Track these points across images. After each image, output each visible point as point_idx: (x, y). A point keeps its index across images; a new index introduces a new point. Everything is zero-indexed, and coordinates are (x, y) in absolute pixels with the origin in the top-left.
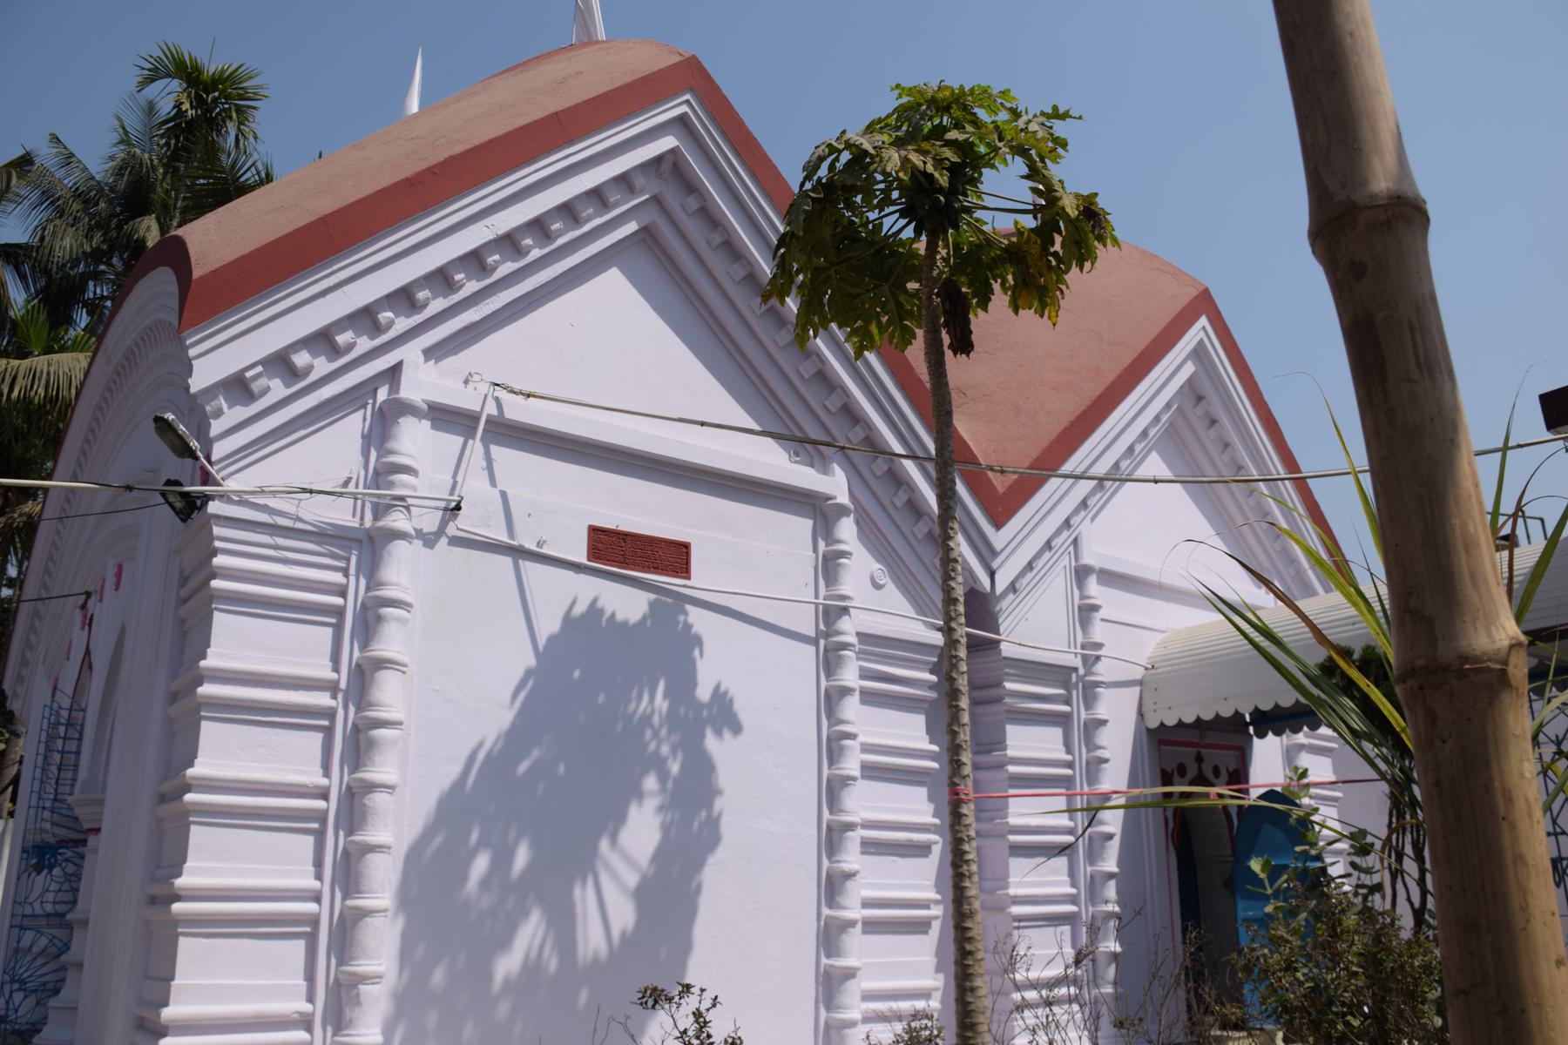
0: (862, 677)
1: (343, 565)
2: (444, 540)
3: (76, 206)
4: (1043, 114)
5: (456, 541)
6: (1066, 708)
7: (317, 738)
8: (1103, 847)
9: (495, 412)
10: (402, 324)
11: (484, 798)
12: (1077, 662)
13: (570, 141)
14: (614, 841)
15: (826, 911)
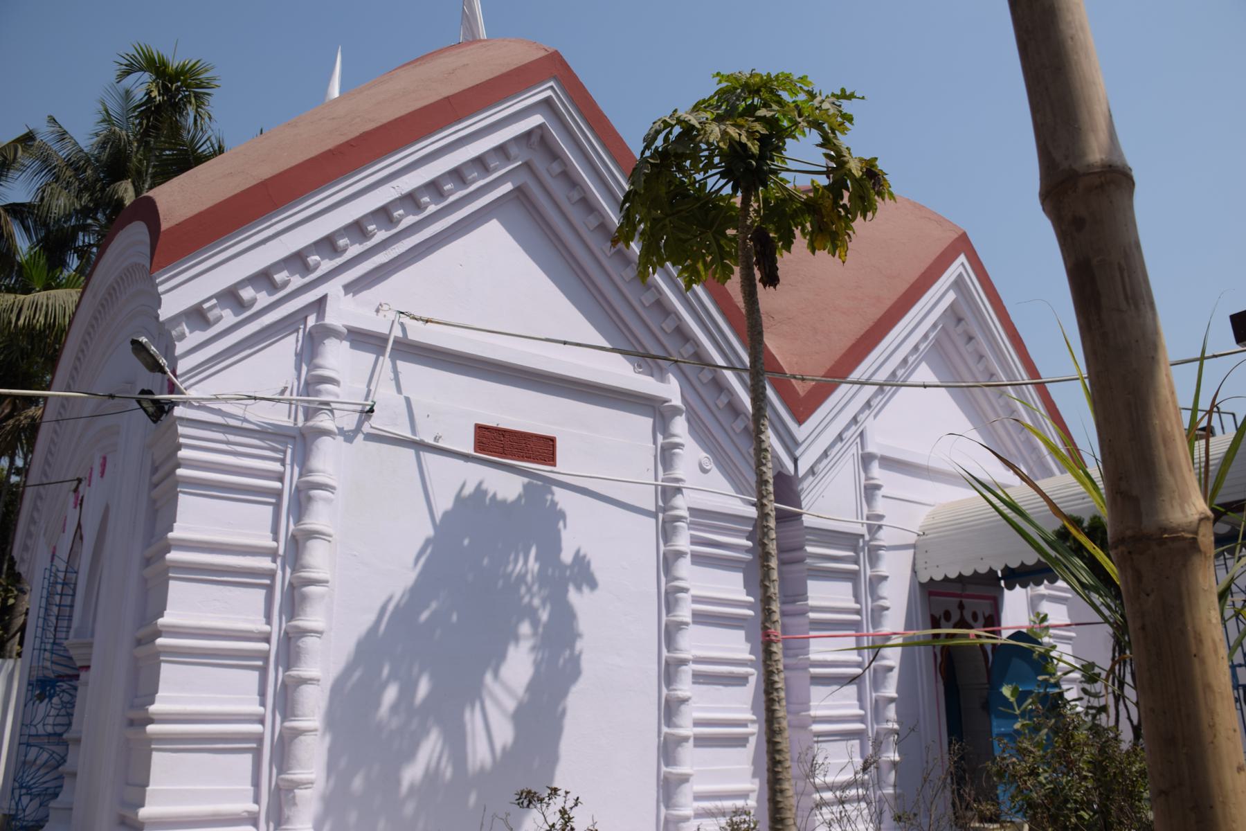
0: (693, 543)
1: (280, 456)
2: (360, 437)
3: (68, 173)
4: (833, 95)
5: (370, 437)
7: (262, 593)
8: (885, 678)
9: (400, 335)
10: (327, 265)
11: (392, 642)
13: (459, 119)
15: (665, 729)
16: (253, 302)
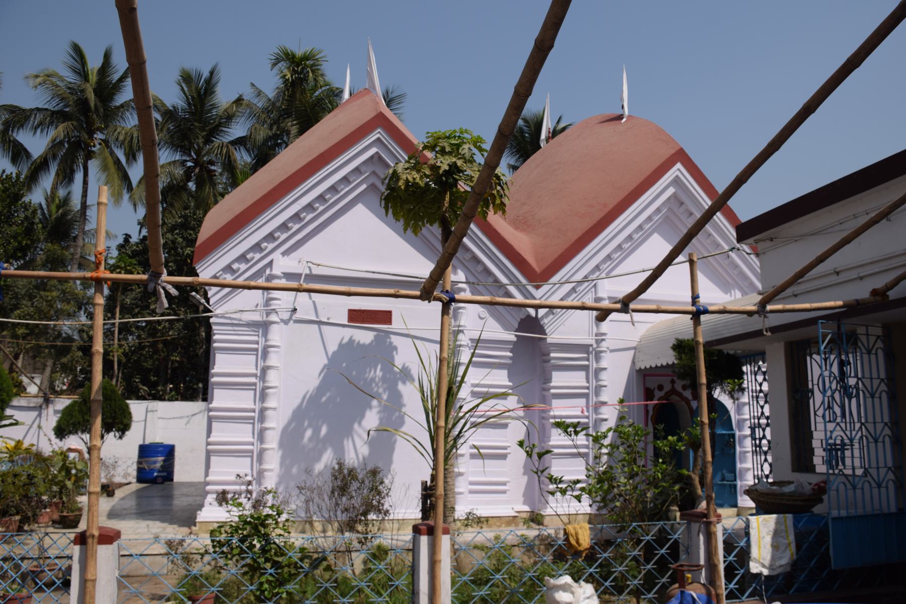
6: (586, 363)
7: (253, 392)
10: (271, 246)
11: (309, 411)
12: (593, 342)
14: (360, 423)
16: (239, 269)
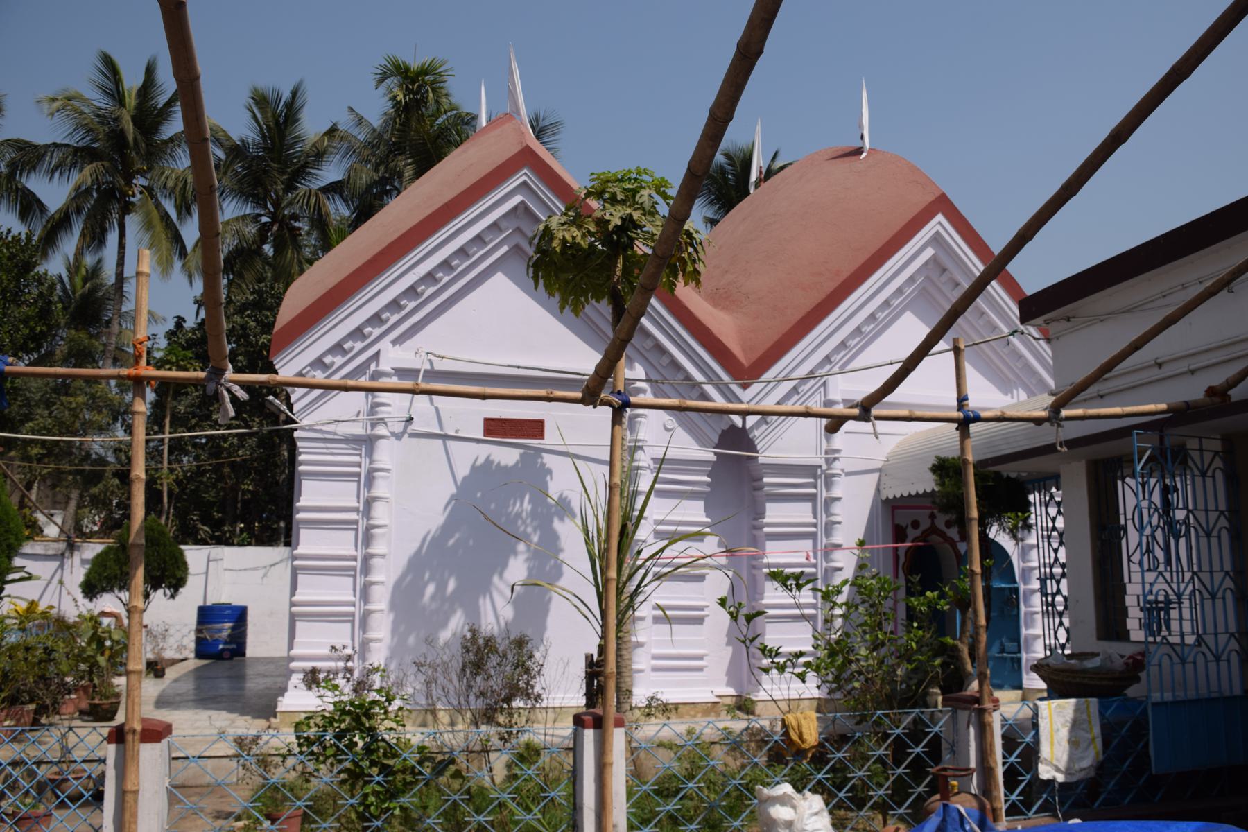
2: (406, 436)
6: (813, 491)
7: (353, 533)
10: (377, 332)
11: (429, 559)
16: (333, 363)
